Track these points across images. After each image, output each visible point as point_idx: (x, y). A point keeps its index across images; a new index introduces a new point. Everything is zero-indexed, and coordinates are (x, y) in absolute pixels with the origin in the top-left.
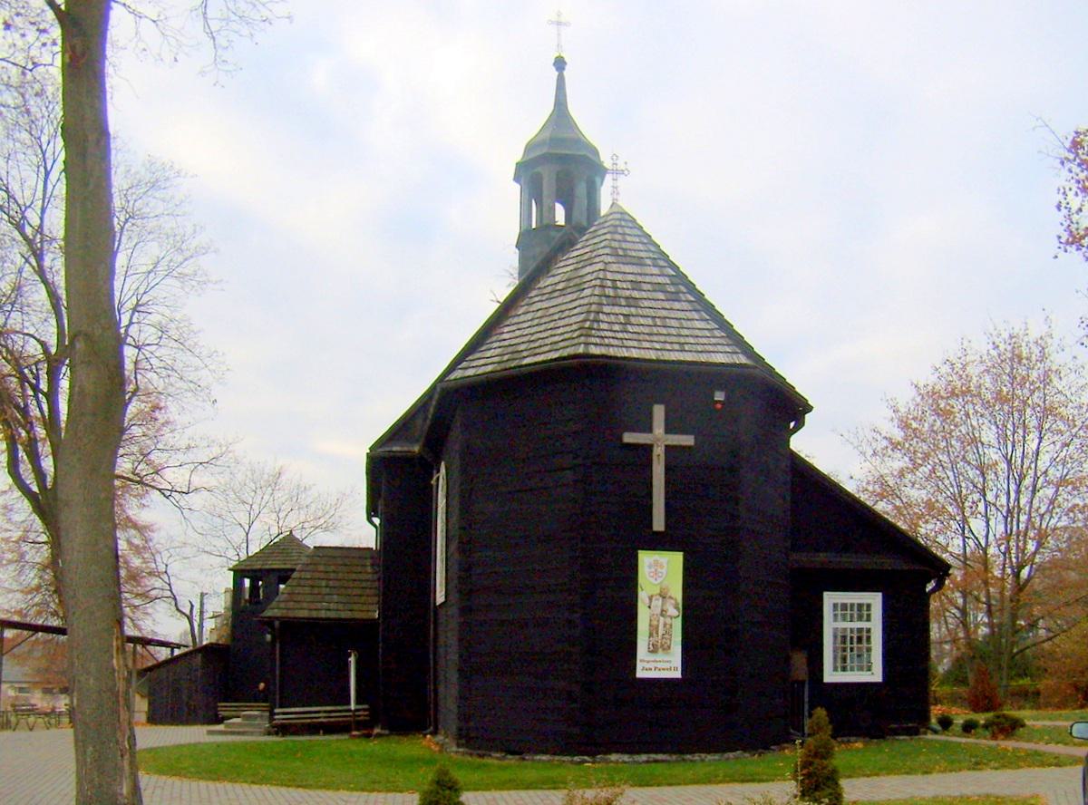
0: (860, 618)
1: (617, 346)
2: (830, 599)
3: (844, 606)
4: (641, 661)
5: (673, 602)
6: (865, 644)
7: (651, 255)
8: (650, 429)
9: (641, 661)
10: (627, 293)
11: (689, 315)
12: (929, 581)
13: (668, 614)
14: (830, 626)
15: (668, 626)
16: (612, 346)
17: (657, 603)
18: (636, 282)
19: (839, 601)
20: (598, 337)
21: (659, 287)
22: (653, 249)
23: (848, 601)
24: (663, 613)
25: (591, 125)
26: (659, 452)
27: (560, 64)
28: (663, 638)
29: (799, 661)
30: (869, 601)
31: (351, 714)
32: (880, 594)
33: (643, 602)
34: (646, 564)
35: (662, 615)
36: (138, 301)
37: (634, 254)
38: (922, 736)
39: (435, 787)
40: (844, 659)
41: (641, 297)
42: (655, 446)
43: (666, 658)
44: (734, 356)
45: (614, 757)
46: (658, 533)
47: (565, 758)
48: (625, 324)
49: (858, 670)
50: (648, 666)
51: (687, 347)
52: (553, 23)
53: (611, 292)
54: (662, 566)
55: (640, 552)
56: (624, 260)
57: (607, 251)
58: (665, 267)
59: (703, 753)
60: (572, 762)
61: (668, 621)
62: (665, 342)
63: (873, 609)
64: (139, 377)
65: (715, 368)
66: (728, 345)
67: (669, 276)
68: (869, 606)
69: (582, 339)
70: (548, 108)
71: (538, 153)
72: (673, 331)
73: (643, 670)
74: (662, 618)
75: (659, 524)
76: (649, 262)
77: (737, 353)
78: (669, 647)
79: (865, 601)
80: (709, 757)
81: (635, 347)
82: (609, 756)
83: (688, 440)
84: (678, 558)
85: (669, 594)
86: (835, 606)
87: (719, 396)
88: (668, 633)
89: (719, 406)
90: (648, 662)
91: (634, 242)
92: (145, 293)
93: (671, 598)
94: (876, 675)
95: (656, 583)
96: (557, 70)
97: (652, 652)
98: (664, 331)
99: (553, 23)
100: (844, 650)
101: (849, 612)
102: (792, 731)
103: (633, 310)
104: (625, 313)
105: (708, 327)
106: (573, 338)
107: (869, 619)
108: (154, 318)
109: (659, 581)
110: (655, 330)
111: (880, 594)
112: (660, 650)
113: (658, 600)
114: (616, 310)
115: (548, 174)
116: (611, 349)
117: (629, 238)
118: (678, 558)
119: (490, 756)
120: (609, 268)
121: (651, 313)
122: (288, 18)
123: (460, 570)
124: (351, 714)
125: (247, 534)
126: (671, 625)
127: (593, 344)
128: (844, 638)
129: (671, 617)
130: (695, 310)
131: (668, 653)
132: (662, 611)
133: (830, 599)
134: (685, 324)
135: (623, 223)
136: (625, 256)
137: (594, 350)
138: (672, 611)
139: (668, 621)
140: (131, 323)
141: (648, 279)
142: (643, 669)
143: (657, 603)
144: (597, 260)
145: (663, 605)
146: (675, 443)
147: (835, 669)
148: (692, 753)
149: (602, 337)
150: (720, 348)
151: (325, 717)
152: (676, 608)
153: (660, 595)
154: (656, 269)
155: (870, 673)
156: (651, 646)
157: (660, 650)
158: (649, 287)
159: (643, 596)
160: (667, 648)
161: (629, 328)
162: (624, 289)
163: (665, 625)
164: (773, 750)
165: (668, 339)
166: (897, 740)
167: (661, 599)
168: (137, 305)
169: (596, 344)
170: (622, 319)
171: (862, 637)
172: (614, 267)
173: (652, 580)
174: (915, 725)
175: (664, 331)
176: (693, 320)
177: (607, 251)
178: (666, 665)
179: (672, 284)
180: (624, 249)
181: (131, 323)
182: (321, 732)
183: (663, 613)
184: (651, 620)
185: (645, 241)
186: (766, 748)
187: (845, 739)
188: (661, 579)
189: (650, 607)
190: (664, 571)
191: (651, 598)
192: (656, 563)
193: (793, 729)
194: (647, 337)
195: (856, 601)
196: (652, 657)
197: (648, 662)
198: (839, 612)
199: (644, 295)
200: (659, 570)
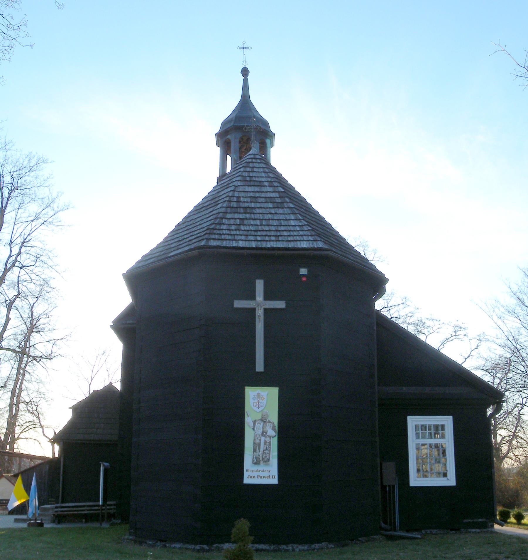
1: (229, 240)
2: (413, 422)
3: (424, 427)
4: (247, 471)
7: (269, 180)
8: (253, 298)
9: (247, 471)
10: (246, 205)
11: (287, 217)
12: (489, 407)
15: (268, 444)
16: (226, 240)
17: (260, 426)
18: (255, 197)
20: (217, 234)
21: (271, 200)
22: (271, 175)
24: (264, 433)
26: (260, 313)
27: (245, 72)
28: (263, 453)
29: (389, 468)
30: (443, 423)
31: (100, 508)
36: (25, 240)
37: (257, 179)
38: (490, 529)
39: (378, 535)
41: (255, 206)
42: (257, 309)
44: (315, 243)
47: (190, 546)
48: (240, 225)
49: (423, 477)
50: (252, 474)
51: (280, 238)
52: (240, 48)
53: (234, 204)
54: (263, 399)
55: (246, 387)
56: (249, 183)
57: (239, 178)
58: (277, 186)
59: (294, 543)
60: (194, 550)
61: (268, 439)
62: (266, 236)
63: (446, 428)
64: (20, 285)
66: (311, 235)
67: (279, 192)
68: (443, 427)
69: (206, 236)
71: (228, 126)
72: (273, 228)
73: (248, 477)
74: (263, 439)
75: (260, 367)
76: (266, 184)
77: (317, 240)
78: (268, 460)
79: (440, 423)
80: (300, 547)
81: (242, 240)
82: (222, 545)
83: (280, 304)
84: (274, 392)
86: (416, 426)
88: (268, 449)
89: (304, 279)
90: (252, 471)
91: (259, 172)
92: (29, 235)
93: (269, 422)
94: (451, 481)
95: (258, 411)
97: (255, 464)
98: (267, 228)
99: (240, 48)
101: (427, 431)
103: (248, 216)
104: (241, 217)
105: (300, 224)
106: (202, 236)
108: (33, 251)
109: (260, 409)
110: (260, 228)
112: (262, 462)
113: (260, 424)
114: (236, 216)
115: (234, 139)
116: (225, 242)
117: (256, 170)
118: (274, 392)
119: (146, 543)
120: (237, 189)
121: (261, 216)
122: (31, 46)
124: (100, 508)
125: (90, 385)
126: (270, 443)
127: (213, 239)
129: (270, 437)
130: (292, 214)
131: (268, 465)
132: (263, 432)
133: (413, 422)
134: (283, 223)
135: (254, 160)
136: (250, 181)
137: (213, 243)
138: (271, 432)
139: (268, 439)
140: (20, 253)
141: (263, 195)
143: (260, 426)
144: (231, 185)
145: (264, 427)
148: (287, 543)
149: (221, 234)
150: (305, 238)
151: (88, 510)
152: (274, 429)
153: (262, 420)
154: (271, 188)
155: (445, 478)
156: (255, 459)
157: (262, 462)
158: (263, 200)
159: (248, 420)
160: (267, 461)
161: (242, 228)
162: (244, 202)
163: (265, 442)
165: (268, 233)
166: (470, 532)
168: (24, 242)
169: (214, 239)
170: (238, 222)
172: (241, 189)
174: (484, 520)
175: (267, 228)
176: (289, 220)
177: (239, 178)
178: (266, 474)
179: (280, 197)
180: (250, 177)
181: (20, 253)
182: (84, 520)
183: (264, 433)
184: (254, 439)
185: (267, 171)
188: (263, 407)
189: (254, 429)
190: (264, 402)
191: (254, 422)
194: (253, 233)
195: (433, 423)
196: (256, 468)
197: (252, 471)
198: (420, 432)
199: (258, 205)
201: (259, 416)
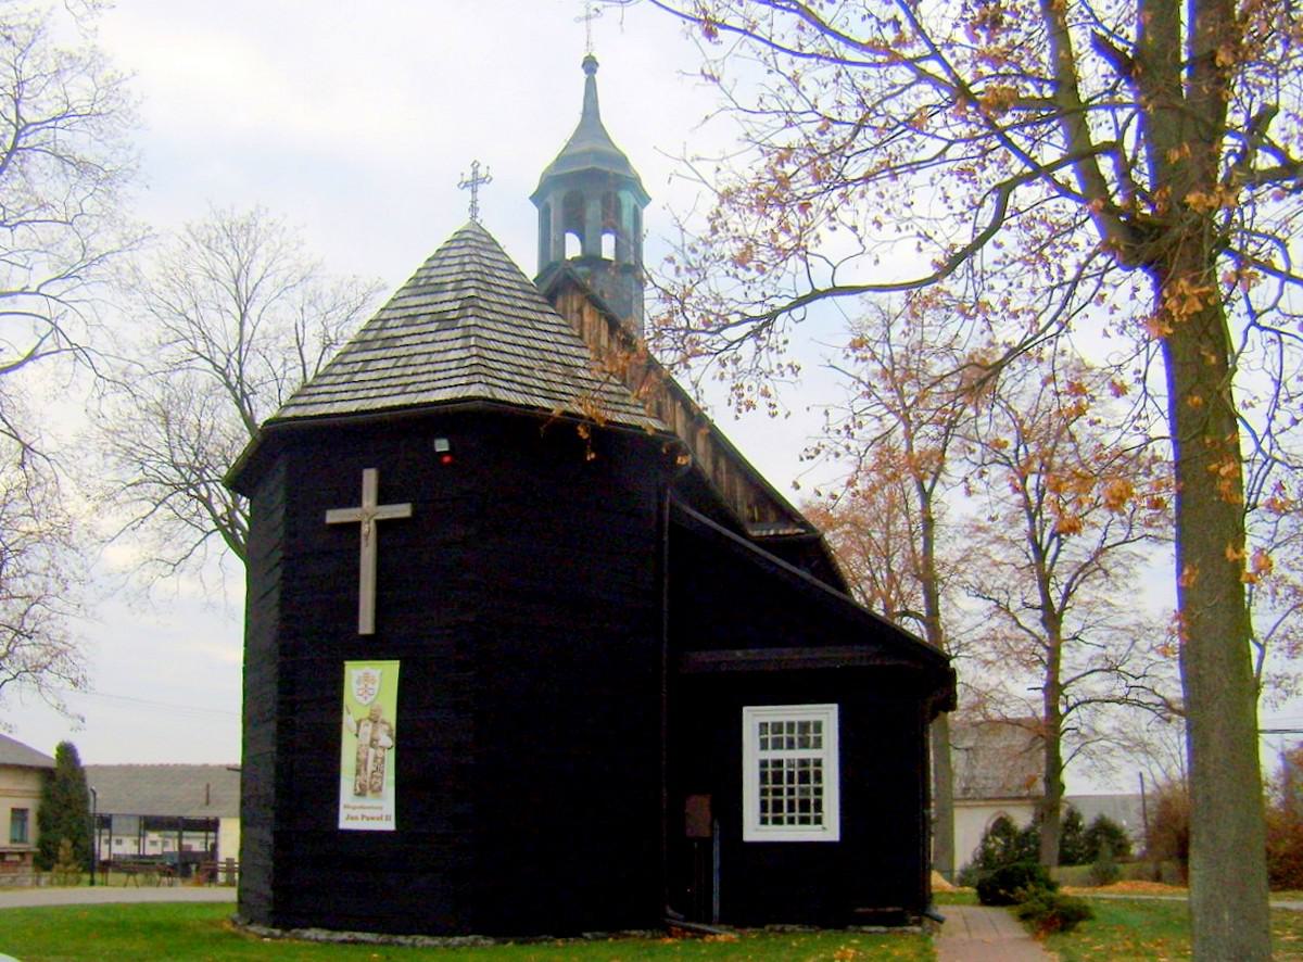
0: (804, 744)
2: (753, 718)
3: (778, 727)
4: (345, 807)
5: (386, 727)
6: (812, 785)
9: (345, 807)
13: (381, 743)
14: (752, 757)
17: (367, 729)
19: (770, 720)
23: (785, 719)
24: (373, 743)
25: (627, 134)
26: (368, 529)
27: (590, 65)
28: (372, 777)
32: (835, 707)
33: (350, 730)
34: (355, 678)
35: (372, 746)
40: (778, 806)
43: (376, 803)
45: (311, 933)
46: (366, 637)
50: (354, 813)
61: (380, 752)
65: (351, 418)
68: (818, 726)
70: (573, 119)
74: (372, 751)
75: (366, 625)
78: (380, 789)
79: (811, 718)
85: (382, 717)
86: (763, 726)
87: (442, 445)
88: (379, 769)
89: (447, 459)
90: (354, 808)
93: (384, 722)
94: (829, 829)
96: (586, 72)
97: (359, 795)
100: (778, 792)
102: (670, 912)
107: (818, 744)
109: (369, 700)
111: (835, 707)
112: (369, 793)
123: (280, 692)
128: (778, 778)
129: (383, 748)
131: (379, 797)
132: (372, 740)
133: (753, 718)
142: (348, 817)
146: (387, 516)
147: (764, 821)
152: (390, 736)
153: (370, 719)
155: (819, 826)
159: (349, 720)
163: (376, 758)
164: (586, 938)
167: (371, 724)
171: (808, 774)
173: (361, 699)
178: (376, 813)
183: (373, 743)
184: (358, 753)
186: (577, 934)
187: (778, 927)
190: (376, 686)
191: (358, 724)
192: (367, 677)
193: (673, 908)
196: (360, 802)
197: (354, 808)
198: (770, 736)
200: (370, 686)
201: (365, 713)
